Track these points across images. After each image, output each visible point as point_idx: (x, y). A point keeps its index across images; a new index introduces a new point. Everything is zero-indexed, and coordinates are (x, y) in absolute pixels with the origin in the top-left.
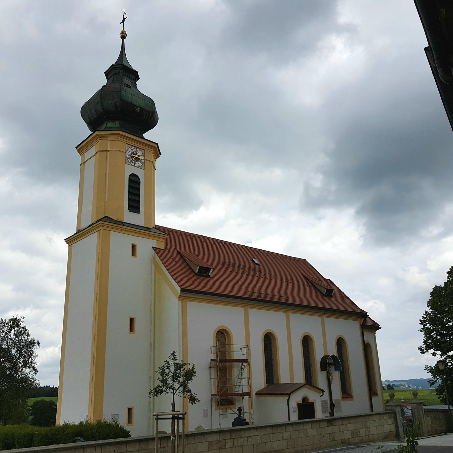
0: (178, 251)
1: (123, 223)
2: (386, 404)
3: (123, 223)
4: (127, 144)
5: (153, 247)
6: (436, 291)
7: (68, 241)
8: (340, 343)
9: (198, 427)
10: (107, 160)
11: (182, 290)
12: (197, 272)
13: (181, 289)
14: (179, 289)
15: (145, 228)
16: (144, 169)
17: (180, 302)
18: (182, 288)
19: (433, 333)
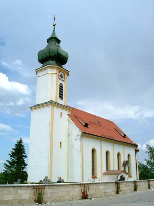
8: (129, 156)
11: (83, 133)
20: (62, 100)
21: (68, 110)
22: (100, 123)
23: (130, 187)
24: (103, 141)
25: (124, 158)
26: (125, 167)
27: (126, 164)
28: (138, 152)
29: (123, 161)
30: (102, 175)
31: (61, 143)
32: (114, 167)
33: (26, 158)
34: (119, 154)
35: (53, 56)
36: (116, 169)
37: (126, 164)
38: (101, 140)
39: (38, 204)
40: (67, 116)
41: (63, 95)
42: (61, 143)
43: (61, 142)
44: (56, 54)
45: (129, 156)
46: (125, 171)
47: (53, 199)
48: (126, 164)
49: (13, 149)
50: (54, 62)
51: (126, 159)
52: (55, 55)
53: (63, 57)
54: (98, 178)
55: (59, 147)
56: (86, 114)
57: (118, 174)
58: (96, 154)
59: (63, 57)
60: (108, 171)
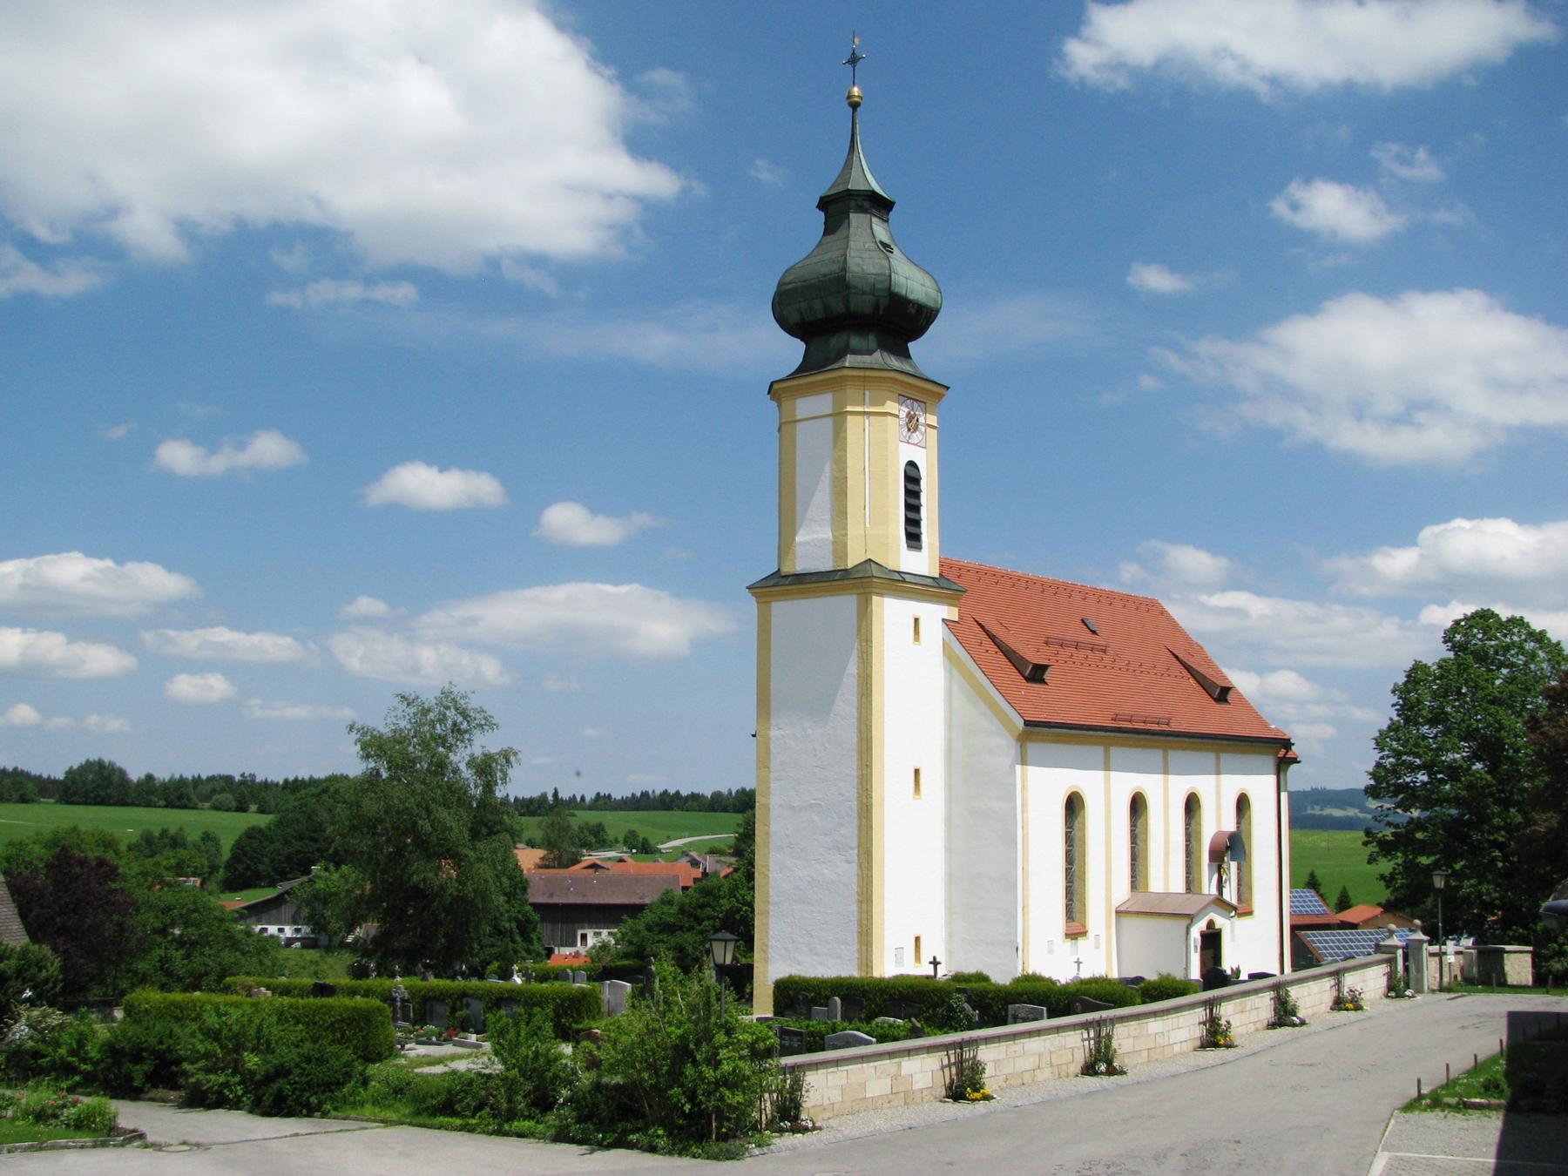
0: (976, 621)
1: (903, 575)
2: (1390, 955)
3: (903, 575)
4: (900, 395)
5: (943, 620)
6: (1416, 675)
7: (760, 590)
8: (1243, 804)
9: (667, 892)
10: (864, 434)
11: (1027, 723)
12: (1026, 674)
13: (1025, 721)
14: (1020, 723)
15: (929, 580)
16: (925, 448)
17: (1019, 744)
18: (1026, 719)
19: (1496, 839)
20: (919, 548)
23: (1255, 1012)
24: (1116, 744)
25: (1217, 821)
26: (1220, 867)
27: (1228, 848)
28: (1294, 767)
29: (1215, 831)
31: (917, 772)
32: (1166, 874)
33: (256, 773)
35: (868, 310)
36: (1178, 885)
37: (1232, 847)
42: (917, 772)
44: (883, 302)
45: (1243, 804)
46: (1220, 902)
48: (1232, 847)
50: (872, 340)
51: (1230, 825)
52: (876, 307)
54: (1091, 934)
55: (1450, 1066)
57: (1191, 918)
59: (914, 311)
60: (1140, 896)
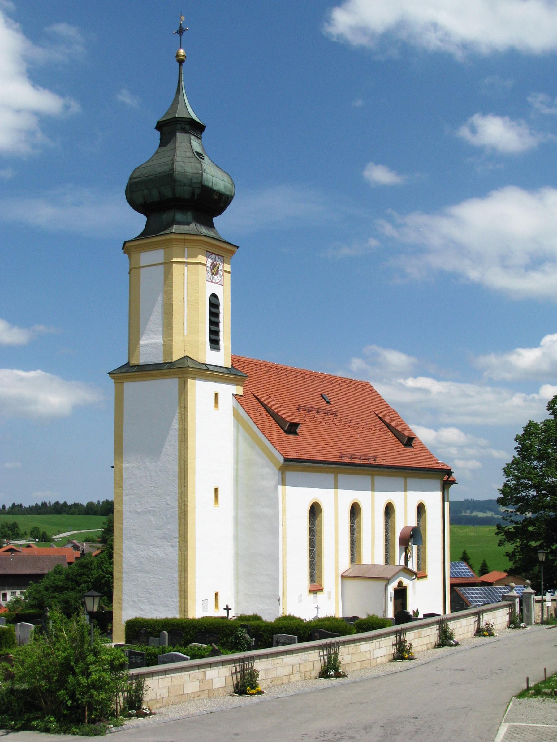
8: (421, 509)
11: (286, 460)
20: (218, 349)
21: (315, 521)
22: (328, 403)
27: (411, 537)
30: (336, 580)
34: (389, 510)
36: (380, 560)
38: (336, 473)
39: (235, 696)
40: (231, 398)
41: (221, 334)
43: (216, 486)
44: (197, 191)
45: (421, 509)
46: (406, 570)
47: (269, 683)
49: (50, 502)
51: (412, 522)
53: (216, 197)
54: (325, 591)
56: (283, 372)
57: (388, 580)
58: (321, 522)
